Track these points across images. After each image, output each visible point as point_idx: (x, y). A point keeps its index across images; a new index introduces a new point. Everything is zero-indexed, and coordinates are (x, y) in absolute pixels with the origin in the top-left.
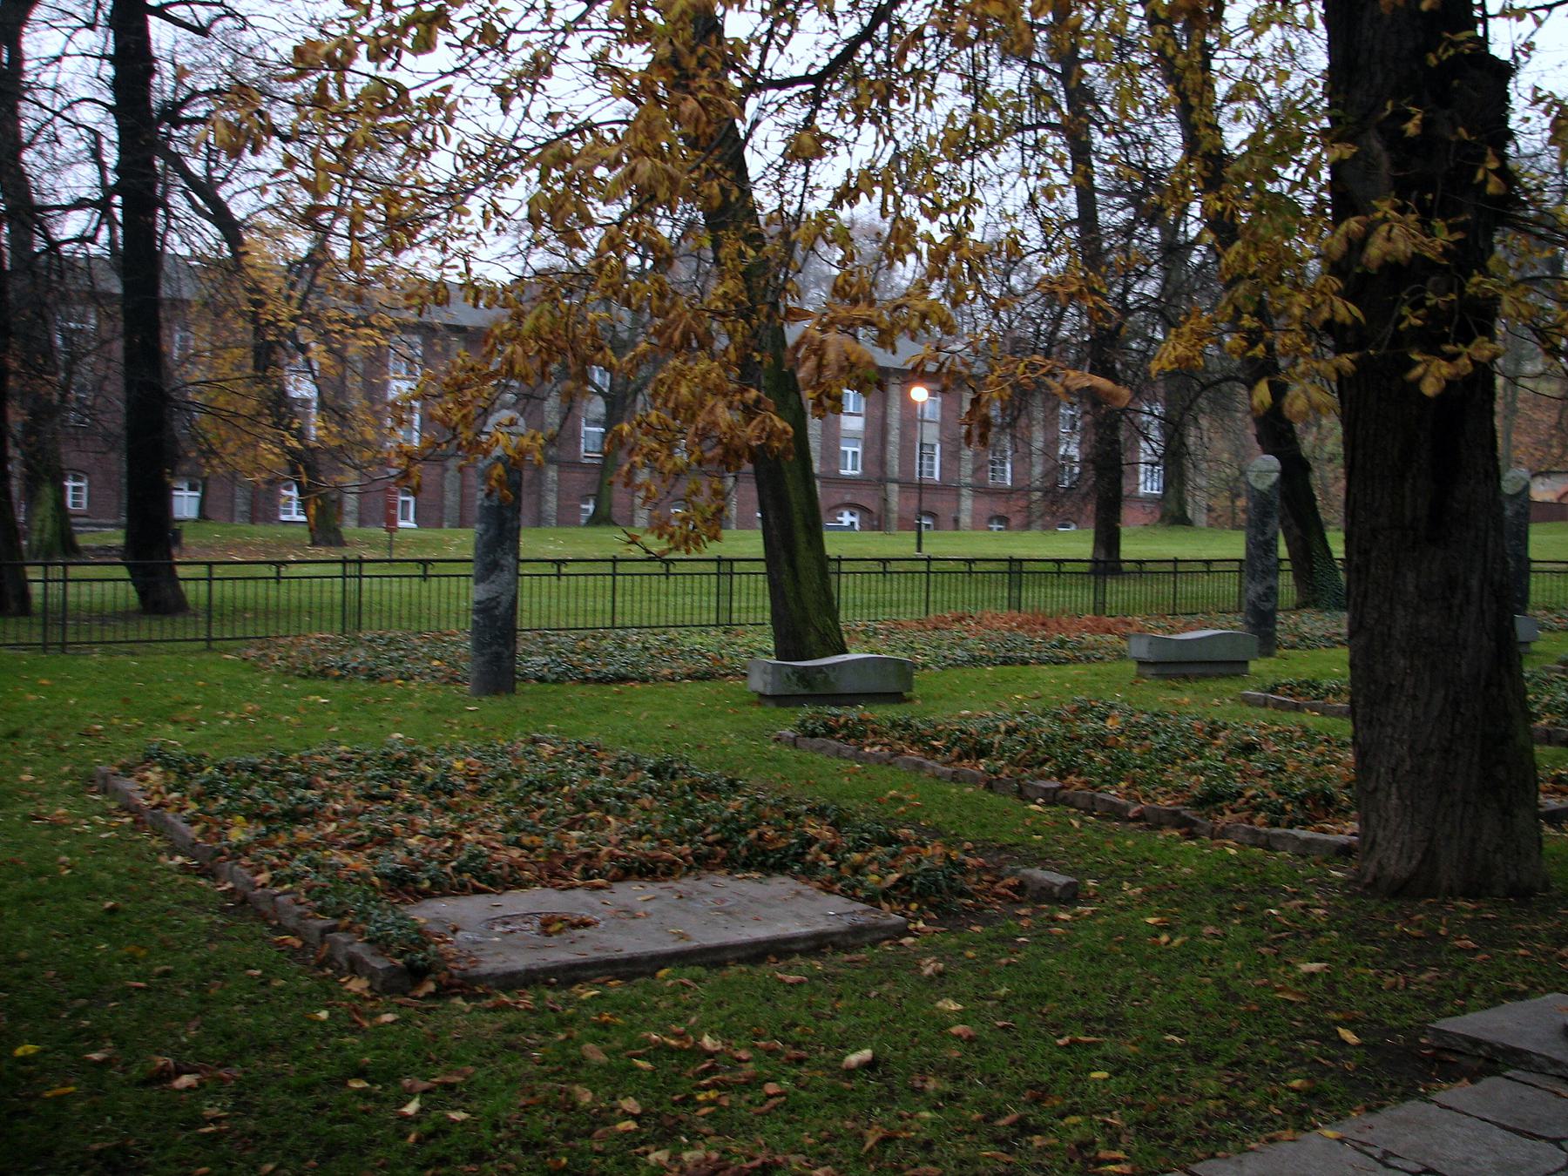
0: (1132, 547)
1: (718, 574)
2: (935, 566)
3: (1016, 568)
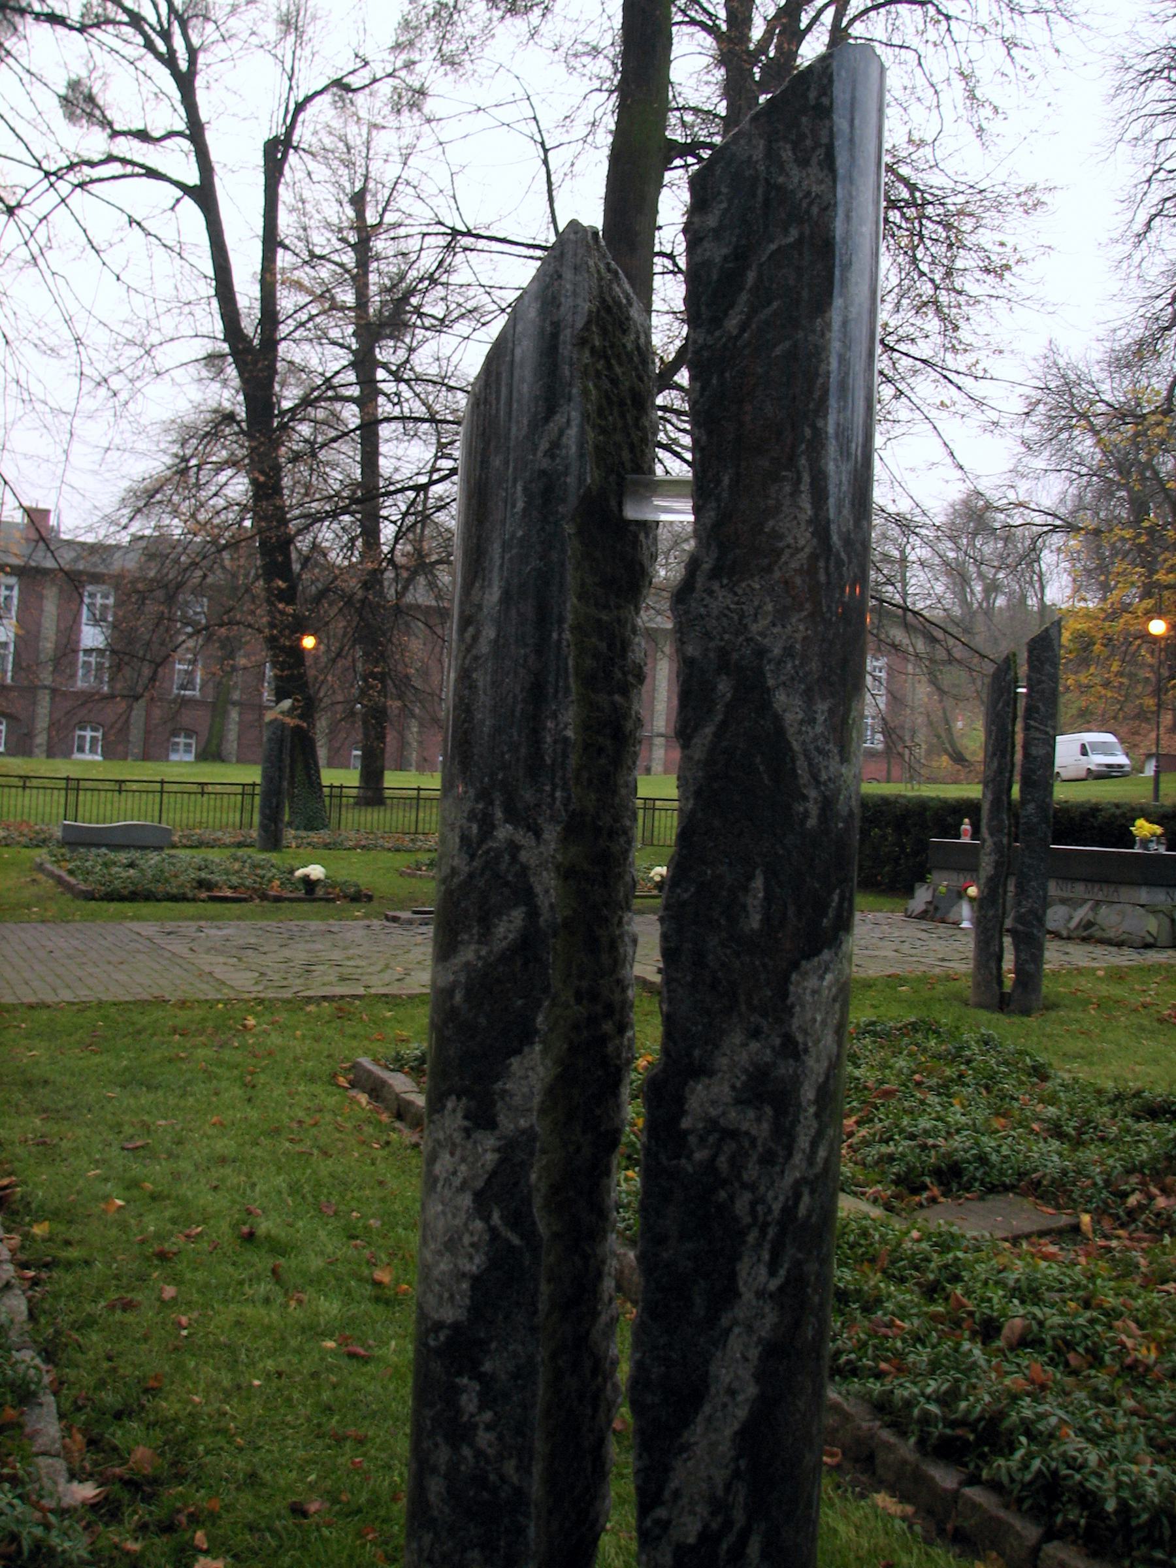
0: (392, 780)
1: (243, 794)
2: (167, 787)
3: (73, 784)
